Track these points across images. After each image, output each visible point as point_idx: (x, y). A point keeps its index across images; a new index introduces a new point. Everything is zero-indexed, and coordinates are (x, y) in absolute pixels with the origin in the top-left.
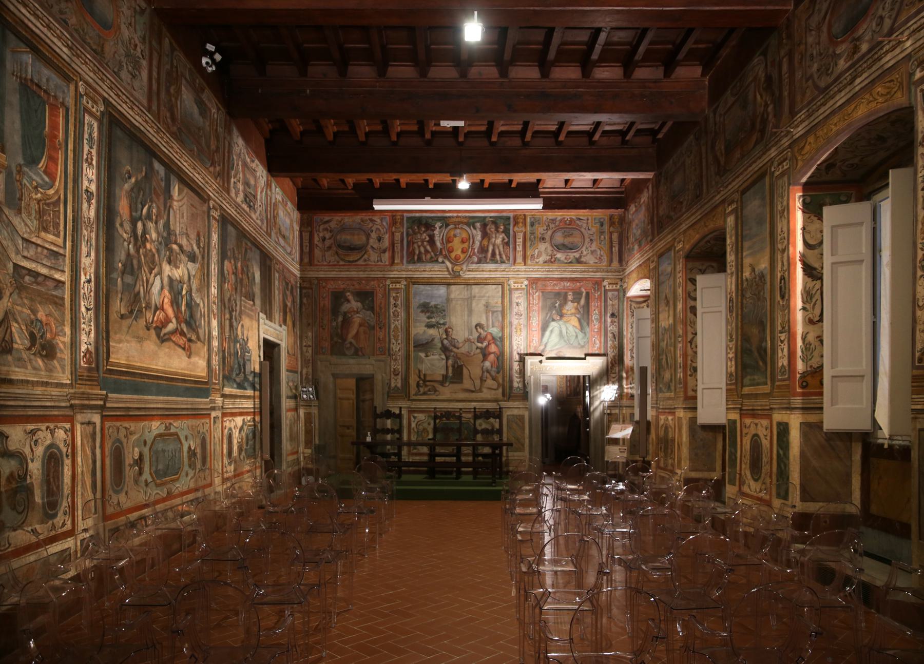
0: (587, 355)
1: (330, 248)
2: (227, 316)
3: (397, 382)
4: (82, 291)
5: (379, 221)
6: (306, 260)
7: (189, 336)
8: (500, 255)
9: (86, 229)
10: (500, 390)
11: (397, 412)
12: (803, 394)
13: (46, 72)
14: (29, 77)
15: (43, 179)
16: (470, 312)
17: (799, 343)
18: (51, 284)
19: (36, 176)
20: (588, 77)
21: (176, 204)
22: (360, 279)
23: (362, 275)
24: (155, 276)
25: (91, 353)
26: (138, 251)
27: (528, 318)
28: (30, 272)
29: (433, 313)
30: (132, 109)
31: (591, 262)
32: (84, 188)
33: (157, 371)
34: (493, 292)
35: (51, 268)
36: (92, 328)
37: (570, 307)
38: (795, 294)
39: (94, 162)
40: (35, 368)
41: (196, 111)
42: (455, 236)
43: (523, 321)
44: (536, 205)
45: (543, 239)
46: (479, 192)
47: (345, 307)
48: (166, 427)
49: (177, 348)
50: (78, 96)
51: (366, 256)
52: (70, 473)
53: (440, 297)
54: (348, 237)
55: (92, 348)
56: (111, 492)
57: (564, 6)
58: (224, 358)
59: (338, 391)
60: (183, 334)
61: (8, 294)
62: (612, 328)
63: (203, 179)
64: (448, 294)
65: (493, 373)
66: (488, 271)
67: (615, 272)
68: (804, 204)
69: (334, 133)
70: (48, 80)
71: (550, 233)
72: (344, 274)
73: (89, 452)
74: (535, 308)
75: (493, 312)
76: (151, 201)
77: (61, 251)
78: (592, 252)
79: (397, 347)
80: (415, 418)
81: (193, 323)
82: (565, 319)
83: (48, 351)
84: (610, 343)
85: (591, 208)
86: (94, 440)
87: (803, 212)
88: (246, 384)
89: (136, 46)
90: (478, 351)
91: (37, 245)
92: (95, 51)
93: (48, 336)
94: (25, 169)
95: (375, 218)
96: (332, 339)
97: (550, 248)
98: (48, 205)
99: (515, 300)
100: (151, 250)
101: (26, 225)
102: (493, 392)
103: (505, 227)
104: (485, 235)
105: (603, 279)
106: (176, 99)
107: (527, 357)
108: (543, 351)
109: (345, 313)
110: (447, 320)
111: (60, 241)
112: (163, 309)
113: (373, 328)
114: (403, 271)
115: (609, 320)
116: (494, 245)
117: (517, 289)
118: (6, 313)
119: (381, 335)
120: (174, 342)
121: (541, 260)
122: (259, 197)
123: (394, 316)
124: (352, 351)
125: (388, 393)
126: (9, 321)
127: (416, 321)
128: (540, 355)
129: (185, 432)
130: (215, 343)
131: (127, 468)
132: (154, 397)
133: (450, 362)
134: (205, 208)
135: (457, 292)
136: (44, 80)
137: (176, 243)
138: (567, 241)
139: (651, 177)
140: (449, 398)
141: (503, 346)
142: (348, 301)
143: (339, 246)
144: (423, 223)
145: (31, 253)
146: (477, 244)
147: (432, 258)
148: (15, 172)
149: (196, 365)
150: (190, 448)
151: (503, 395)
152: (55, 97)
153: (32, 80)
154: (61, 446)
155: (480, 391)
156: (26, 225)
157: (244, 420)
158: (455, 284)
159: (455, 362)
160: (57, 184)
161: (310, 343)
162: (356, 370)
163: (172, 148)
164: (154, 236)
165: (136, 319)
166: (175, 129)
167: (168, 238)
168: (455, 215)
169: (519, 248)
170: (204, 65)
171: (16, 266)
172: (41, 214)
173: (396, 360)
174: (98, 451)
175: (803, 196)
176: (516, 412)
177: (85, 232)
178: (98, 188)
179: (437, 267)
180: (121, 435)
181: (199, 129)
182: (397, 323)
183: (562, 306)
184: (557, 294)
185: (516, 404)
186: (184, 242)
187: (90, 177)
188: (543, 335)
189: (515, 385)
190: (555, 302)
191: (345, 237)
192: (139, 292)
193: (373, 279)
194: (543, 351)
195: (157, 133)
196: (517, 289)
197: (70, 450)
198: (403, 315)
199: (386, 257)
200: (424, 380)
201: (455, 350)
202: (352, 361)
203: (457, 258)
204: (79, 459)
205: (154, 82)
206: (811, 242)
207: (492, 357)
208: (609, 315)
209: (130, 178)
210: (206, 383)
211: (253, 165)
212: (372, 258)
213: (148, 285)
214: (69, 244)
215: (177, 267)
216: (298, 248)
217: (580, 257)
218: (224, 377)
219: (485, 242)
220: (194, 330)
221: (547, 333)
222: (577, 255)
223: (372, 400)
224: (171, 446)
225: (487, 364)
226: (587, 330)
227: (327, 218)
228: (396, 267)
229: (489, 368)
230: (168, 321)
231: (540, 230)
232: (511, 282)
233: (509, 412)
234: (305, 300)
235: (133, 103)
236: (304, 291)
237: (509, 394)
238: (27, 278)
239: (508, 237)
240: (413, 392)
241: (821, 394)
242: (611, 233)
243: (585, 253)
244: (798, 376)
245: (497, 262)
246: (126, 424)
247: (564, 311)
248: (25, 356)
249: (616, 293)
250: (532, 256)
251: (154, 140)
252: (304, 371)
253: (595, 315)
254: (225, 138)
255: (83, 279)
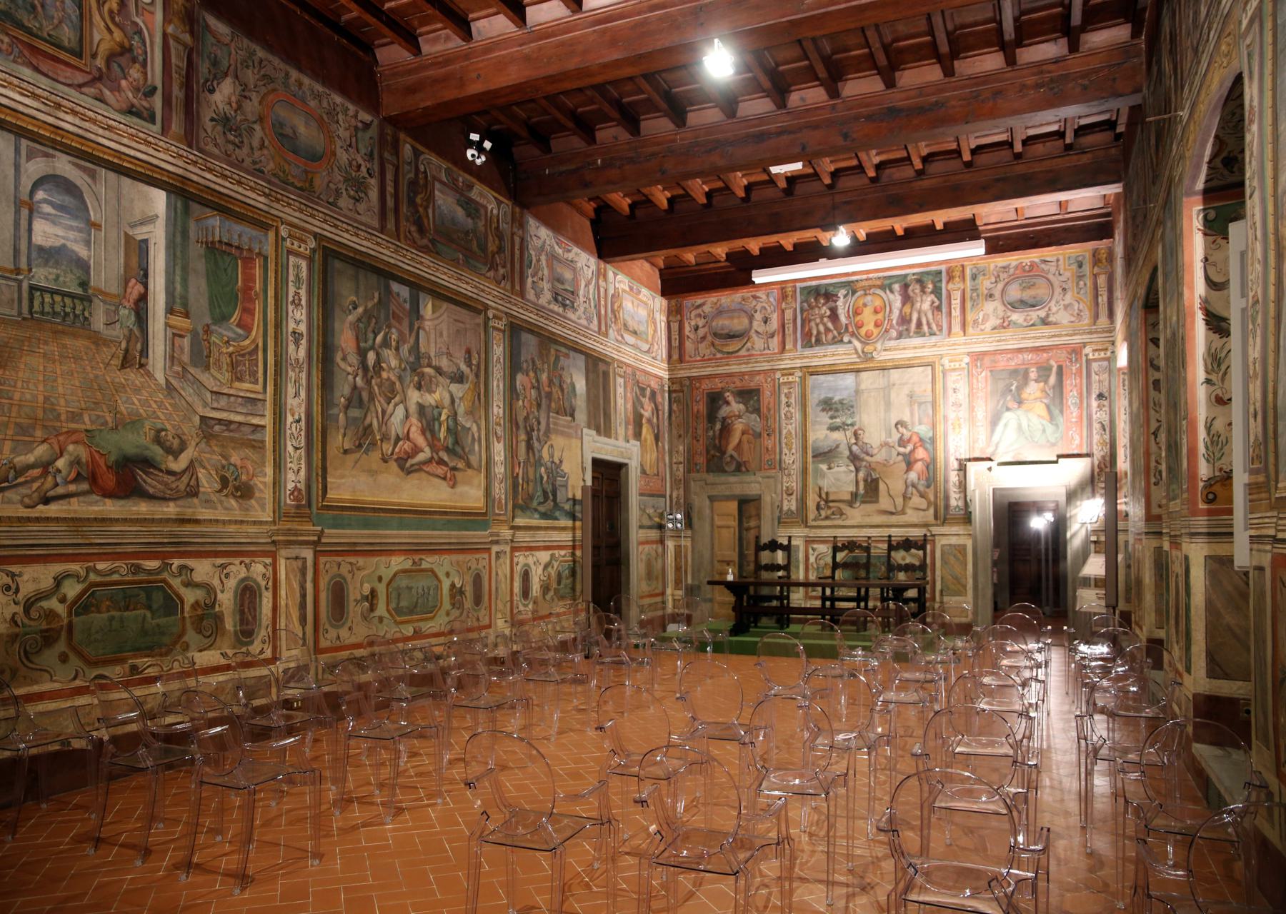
0: (1059, 456)
1: (704, 338)
2: (523, 437)
3: (791, 504)
4: (288, 432)
5: (764, 297)
6: (675, 357)
7: (451, 464)
8: (928, 324)
9: (293, 370)
10: (932, 511)
11: (786, 543)
12: (1210, 513)
13: (238, 228)
14: (217, 238)
15: (235, 333)
16: (888, 405)
17: (1202, 434)
18: (247, 429)
19: (231, 329)
20: (953, 74)
21: (428, 325)
22: (743, 374)
23: (744, 368)
24: (396, 405)
25: (300, 490)
26: (368, 382)
27: (972, 409)
28: (220, 421)
29: (837, 410)
30: (357, 235)
31: (1065, 322)
32: (290, 330)
33: (400, 504)
34: (919, 377)
35: (247, 414)
36: (303, 466)
37: (1033, 389)
38: (1194, 360)
39: (303, 302)
40: (226, 509)
41: (460, 213)
42: (865, 305)
43: (963, 413)
44: (976, 249)
45: (991, 296)
46: (859, 248)
47: (724, 411)
48: (414, 563)
49: (432, 478)
50: (279, 240)
51: (749, 344)
52: (270, 605)
53: (846, 389)
54: (727, 322)
55: (302, 486)
56: (327, 626)
57: (828, 6)
58: (515, 485)
59: (716, 518)
60: (441, 462)
61: (193, 443)
62: (1100, 416)
63: (476, 287)
64: (858, 384)
65: (921, 488)
66: (912, 347)
67: (1104, 332)
68: (1206, 221)
69: (668, 200)
70: (240, 236)
71: (1000, 286)
72: (721, 370)
73: (296, 586)
74: (981, 394)
75: (920, 404)
76: (389, 327)
77: (260, 397)
78: (1066, 307)
79: (791, 458)
80: (814, 550)
81: (458, 449)
82: (1024, 406)
83: (245, 492)
84: (1096, 438)
85: (1059, 243)
86: (304, 574)
87: (1205, 234)
88: (557, 514)
89: (359, 166)
90: (900, 458)
91: (230, 395)
92: (301, 189)
93: (244, 478)
94: (213, 327)
95: (759, 294)
96: (708, 452)
97: (1001, 308)
98: (243, 356)
99: (950, 385)
100: (389, 379)
101: (215, 378)
102: (922, 513)
103: (935, 286)
104: (907, 299)
105: (1085, 345)
106: (426, 208)
107: (969, 464)
108: (993, 453)
109: (724, 419)
110: (856, 419)
111: (259, 387)
112: (408, 437)
113: (760, 435)
114: (798, 357)
115: (1094, 404)
116: (919, 313)
117: (954, 370)
118: (192, 462)
119: (769, 443)
120: (428, 473)
121: (988, 325)
122: (581, 293)
123: (787, 418)
124: (733, 467)
125: (779, 518)
126: (194, 468)
127: (814, 423)
128: (990, 459)
129: (447, 567)
130: (499, 470)
131: (352, 604)
132: (395, 532)
133: (861, 475)
134: (480, 320)
135: (869, 380)
136: (236, 237)
137: (429, 365)
138: (1026, 295)
139: (1120, 190)
140: (860, 523)
141: (935, 449)
142: (728, 403)
143: (715, 335)
144: (822, 293)
145: (223, 402)
146: (896, 313)
147: (834, 337)
148: (201, 332)
149: (471, 495)
150: (453, 585)
151: (936, 517)
152: (250, 250)
153: (220, 242)
154: (260, 579)
155: (903, 512)
156: (215, 378)
157: (552, 555)
158: (866, 370)
159: (869, 475)
160: (254, 333)
161: (681, 459)
162: (738, 490)
163: (421, 263)
164: (394, 363)
165: (366, 452)
166: (425, 242)
167: (417, 362)
168: (864, 277)
169: (956, 313)
170: (470, 158)
171: (203, 419)
172: (233, 366)
173: (789, 475)
174: (309, 586)
175: (1204, 210)
176: (954, 541)
177: (291, 374)
178: (309, 328)
179: (841, 349)
180: (345, 570)
181: (467, 233)
182: (790, 427)
183: (1020, 389)
184: (1014, 372)
185: (955, 529)
186: (444, 363)
187: (298, 319)
188: (993, 431)
189: (953, 503)
190: (1011, 385)
191: (724, 323)
192: (371, 425)
193: (759, 372)
194: (993, 453)
195: (396, 252)
196: (954, 370)
197: (270, 583)
198: (797, 416)
199: (775, 343)
200: (826, 500)
201: (868, 458)
202: (732, 479)
203: (868, 335)
204: (283, 593)
205: (388, 198)
206: (1216, 279)
207: (919, 466)
208: (1094, 396)
209: (355, 308)
210: (485, 514)
211: (570, 256)
212: (756, 347)
213: (385, 417)
214: (270, 389)
215: (431, 391)
216: (664, 342)
217: (1048, 316)
218: (515, 506)
219: (907, 309)
220: (461, 457)
221: (999, 428)
222: (1042, 314)
223: (759, 527)
224: (422, 583)
225: (913, 476)
226: (1060, 420)
227: (699, 302)
228: (787, 355)
229: (916, 480)
230: (417, 450)
231: (986, 284)
232: (946, 361)
233: (944, 541)
234: (675, 407)
235: (359, 228)
236: (674, 395)
237: (943, 515)
238: (217, 428)
239: (940, 299)
240: (811, 516)
241: (1230, 512)
242: (1095, 276)
243: (1054, 309)
244: (1201, 484)
245: (924, 335)
246: (352, 559)
247: (1024, 396)
248: (214, 499)
249: (1105, 363)
250: (975, 322)
251: (392, 261)
252: (675, 495)
253: (1072, 397)
254: (513, 234)
255: (290, 419)
